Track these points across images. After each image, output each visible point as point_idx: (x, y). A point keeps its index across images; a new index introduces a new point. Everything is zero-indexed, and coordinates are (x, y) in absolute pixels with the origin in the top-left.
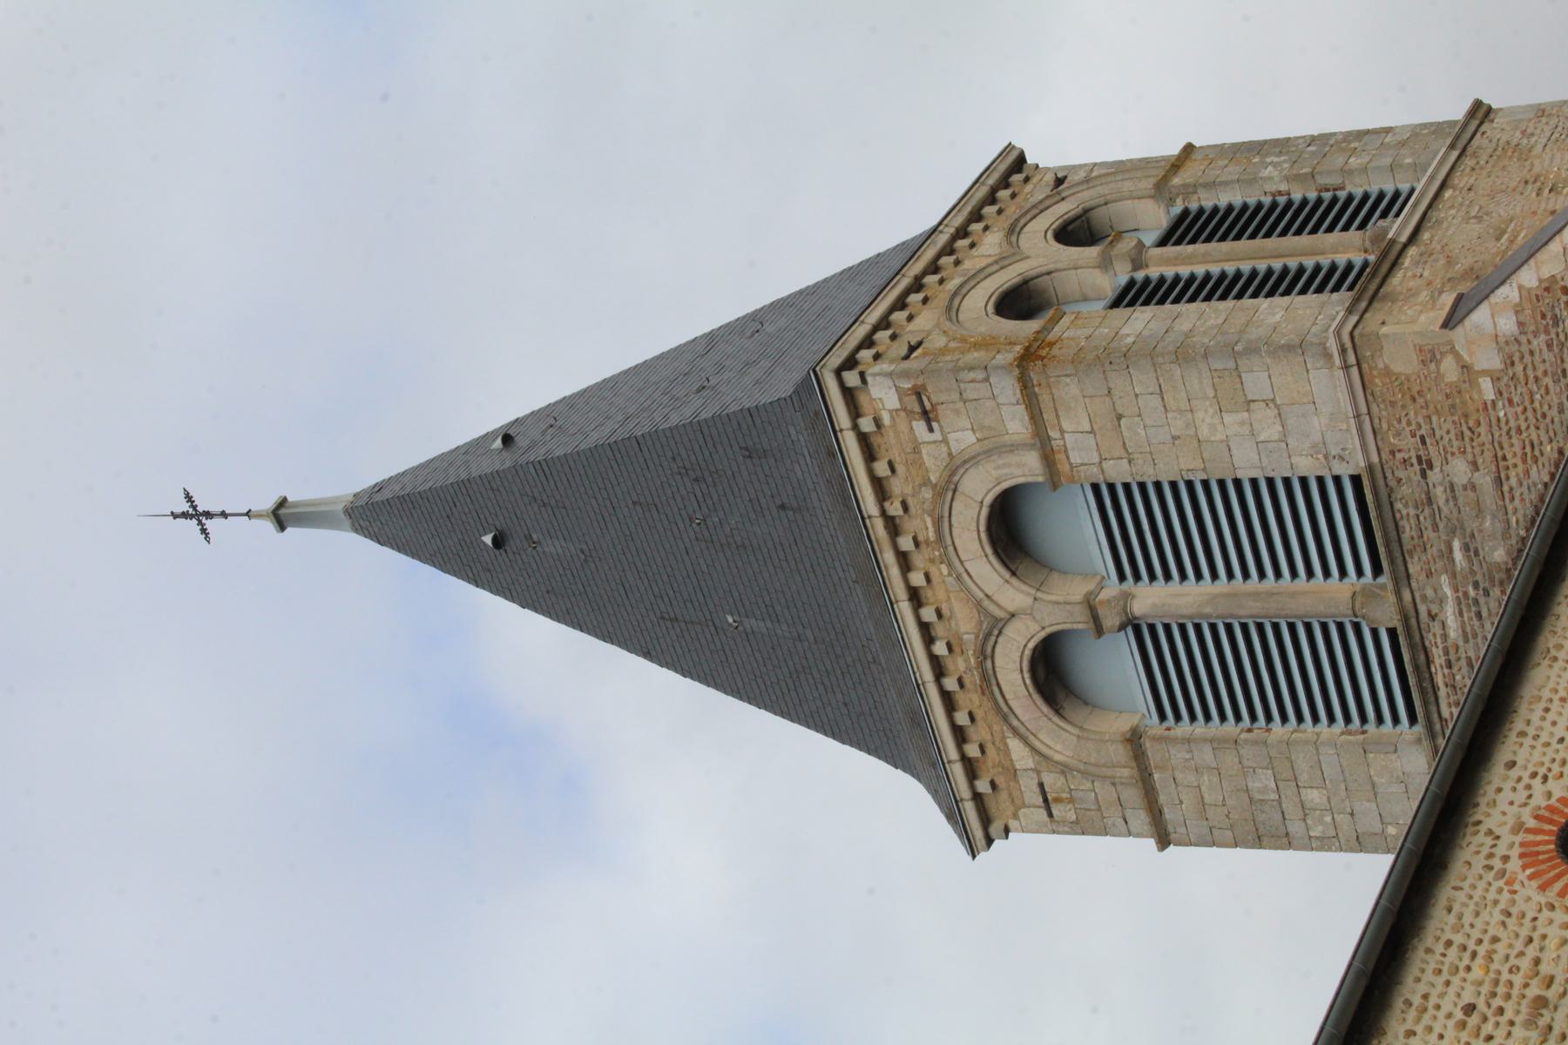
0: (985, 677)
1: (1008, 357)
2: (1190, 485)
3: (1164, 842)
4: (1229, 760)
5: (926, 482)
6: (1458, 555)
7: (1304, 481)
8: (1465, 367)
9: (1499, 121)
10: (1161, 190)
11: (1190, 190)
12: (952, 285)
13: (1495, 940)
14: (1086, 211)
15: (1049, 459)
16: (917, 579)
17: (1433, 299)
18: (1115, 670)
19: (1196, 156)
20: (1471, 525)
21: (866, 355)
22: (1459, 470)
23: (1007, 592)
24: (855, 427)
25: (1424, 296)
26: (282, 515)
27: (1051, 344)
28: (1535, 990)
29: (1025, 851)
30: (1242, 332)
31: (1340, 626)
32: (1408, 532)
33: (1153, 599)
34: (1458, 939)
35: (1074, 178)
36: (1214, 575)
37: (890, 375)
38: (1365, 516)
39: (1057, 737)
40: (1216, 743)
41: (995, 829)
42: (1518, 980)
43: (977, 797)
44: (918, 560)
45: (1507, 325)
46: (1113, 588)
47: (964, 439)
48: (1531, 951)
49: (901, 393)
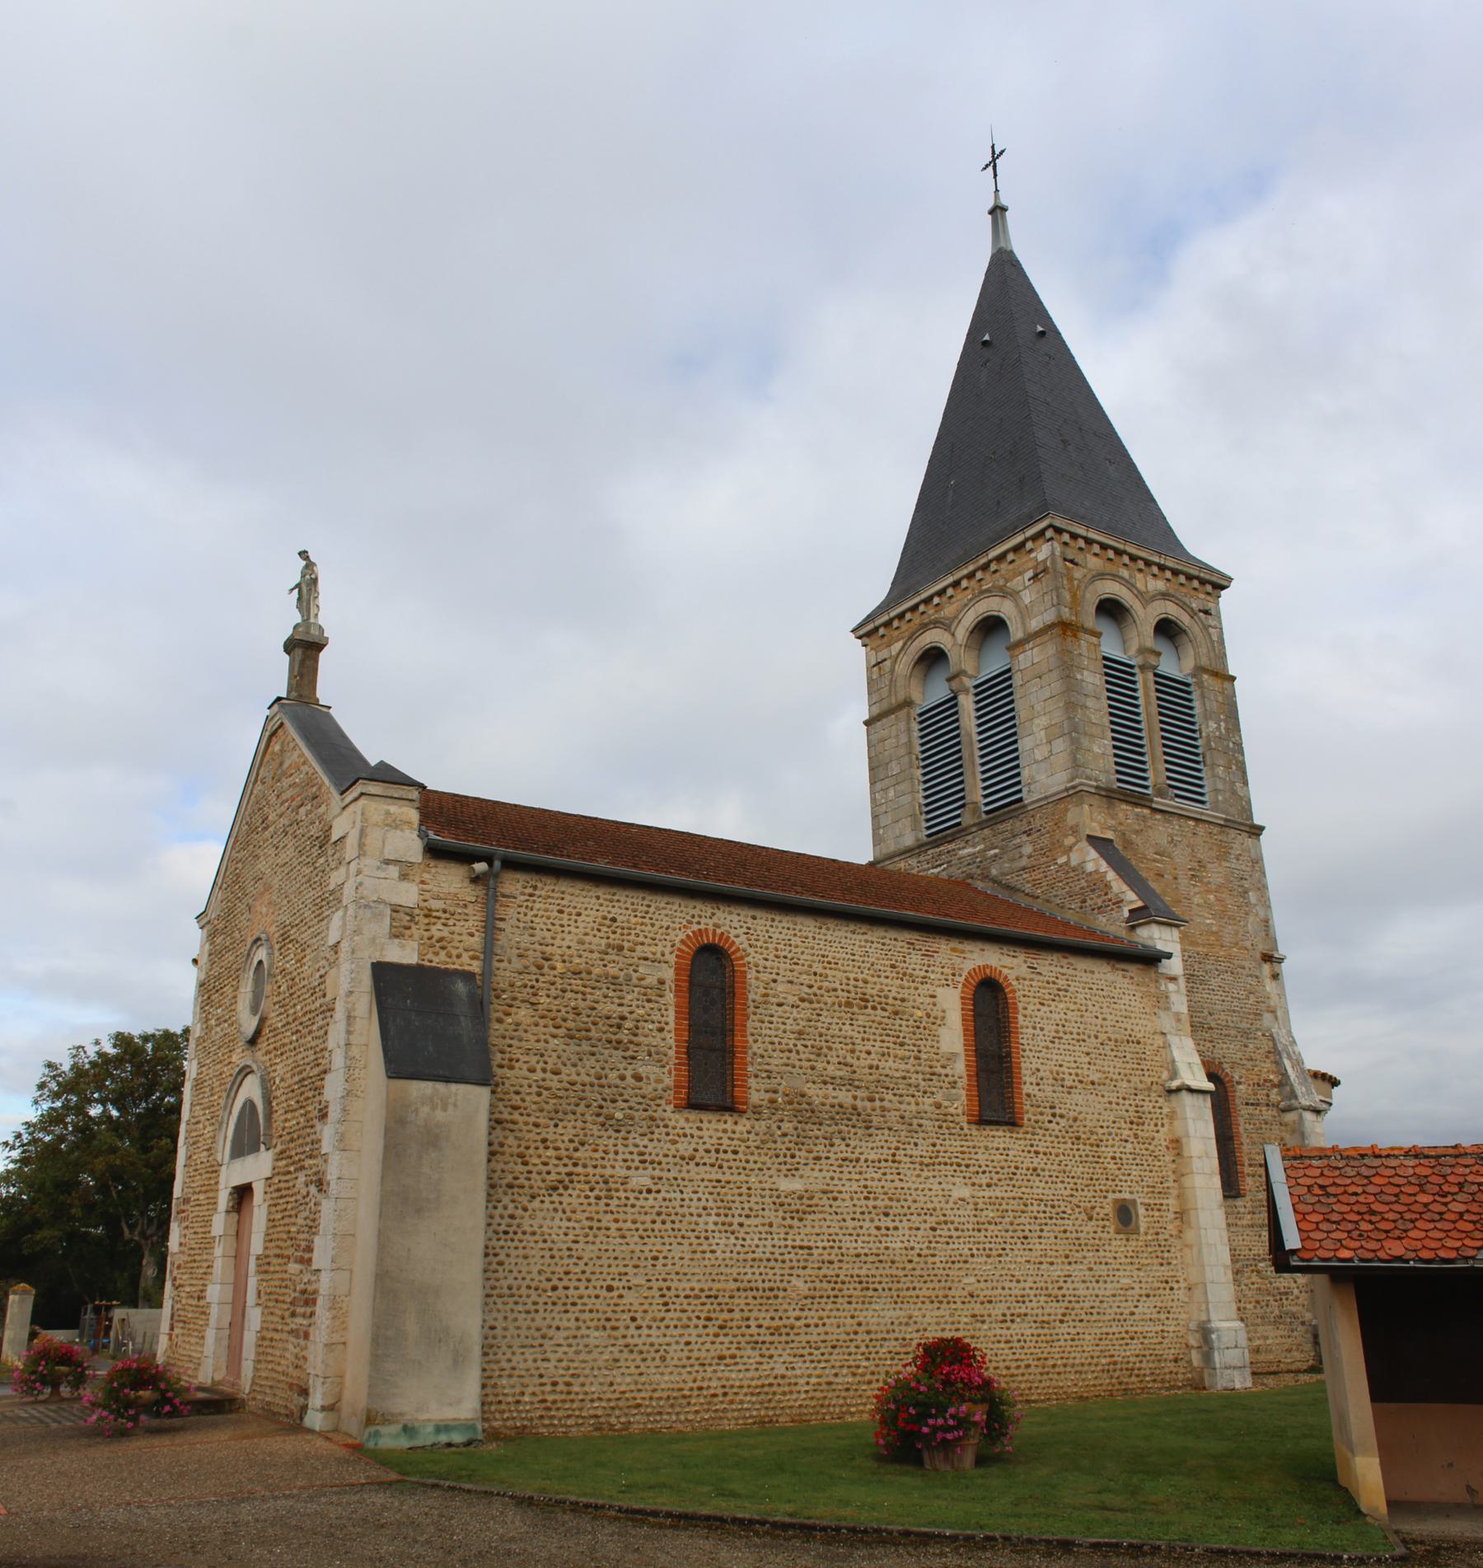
0: (926, 625)
1: (1066, 614)
2: (1013, 718)
3: (867, 723)
4: (902, 751)
5: (1007, 581)
6: (992, 852)
7: (1018, 774)
8: (1071, 848)
9: (1250, 841)
10: (1200, 670)
11: (1200, 685)
12: (1125, 573)
13: (653, 925)
14: (1185, 631)
15: (1020, 643)
16: (964, 583)
17: (1109, 828)
18: (938, 691)
19: (1226, 684)
20: (1005, 858)
21: (1066, 537)
22: (1028, 849)
23: (962, 633)
24: (1027, 540)
25: (1111, 822)
26: (998, 211)
27: (1075, 636)
28: (626, 944)
29: (857, 655)
30: (1086, 734)
31: (963, 798)
32: (1001, 827)
33: (967, 703)
34: (652, 910)
35: (1211, 621)
36: (980, 733)
37: (1053, 554)
38: (1008, 807)
39: (904, 666)
40: (909, 743)
41: (866, 640)
42: (632, 937)
43: (876, 629)
44: (973, 583)
45: (1090, 867)
46: (969, 683)
47: (1027, 597)
48: (648, 941)
49: (1044, 561)
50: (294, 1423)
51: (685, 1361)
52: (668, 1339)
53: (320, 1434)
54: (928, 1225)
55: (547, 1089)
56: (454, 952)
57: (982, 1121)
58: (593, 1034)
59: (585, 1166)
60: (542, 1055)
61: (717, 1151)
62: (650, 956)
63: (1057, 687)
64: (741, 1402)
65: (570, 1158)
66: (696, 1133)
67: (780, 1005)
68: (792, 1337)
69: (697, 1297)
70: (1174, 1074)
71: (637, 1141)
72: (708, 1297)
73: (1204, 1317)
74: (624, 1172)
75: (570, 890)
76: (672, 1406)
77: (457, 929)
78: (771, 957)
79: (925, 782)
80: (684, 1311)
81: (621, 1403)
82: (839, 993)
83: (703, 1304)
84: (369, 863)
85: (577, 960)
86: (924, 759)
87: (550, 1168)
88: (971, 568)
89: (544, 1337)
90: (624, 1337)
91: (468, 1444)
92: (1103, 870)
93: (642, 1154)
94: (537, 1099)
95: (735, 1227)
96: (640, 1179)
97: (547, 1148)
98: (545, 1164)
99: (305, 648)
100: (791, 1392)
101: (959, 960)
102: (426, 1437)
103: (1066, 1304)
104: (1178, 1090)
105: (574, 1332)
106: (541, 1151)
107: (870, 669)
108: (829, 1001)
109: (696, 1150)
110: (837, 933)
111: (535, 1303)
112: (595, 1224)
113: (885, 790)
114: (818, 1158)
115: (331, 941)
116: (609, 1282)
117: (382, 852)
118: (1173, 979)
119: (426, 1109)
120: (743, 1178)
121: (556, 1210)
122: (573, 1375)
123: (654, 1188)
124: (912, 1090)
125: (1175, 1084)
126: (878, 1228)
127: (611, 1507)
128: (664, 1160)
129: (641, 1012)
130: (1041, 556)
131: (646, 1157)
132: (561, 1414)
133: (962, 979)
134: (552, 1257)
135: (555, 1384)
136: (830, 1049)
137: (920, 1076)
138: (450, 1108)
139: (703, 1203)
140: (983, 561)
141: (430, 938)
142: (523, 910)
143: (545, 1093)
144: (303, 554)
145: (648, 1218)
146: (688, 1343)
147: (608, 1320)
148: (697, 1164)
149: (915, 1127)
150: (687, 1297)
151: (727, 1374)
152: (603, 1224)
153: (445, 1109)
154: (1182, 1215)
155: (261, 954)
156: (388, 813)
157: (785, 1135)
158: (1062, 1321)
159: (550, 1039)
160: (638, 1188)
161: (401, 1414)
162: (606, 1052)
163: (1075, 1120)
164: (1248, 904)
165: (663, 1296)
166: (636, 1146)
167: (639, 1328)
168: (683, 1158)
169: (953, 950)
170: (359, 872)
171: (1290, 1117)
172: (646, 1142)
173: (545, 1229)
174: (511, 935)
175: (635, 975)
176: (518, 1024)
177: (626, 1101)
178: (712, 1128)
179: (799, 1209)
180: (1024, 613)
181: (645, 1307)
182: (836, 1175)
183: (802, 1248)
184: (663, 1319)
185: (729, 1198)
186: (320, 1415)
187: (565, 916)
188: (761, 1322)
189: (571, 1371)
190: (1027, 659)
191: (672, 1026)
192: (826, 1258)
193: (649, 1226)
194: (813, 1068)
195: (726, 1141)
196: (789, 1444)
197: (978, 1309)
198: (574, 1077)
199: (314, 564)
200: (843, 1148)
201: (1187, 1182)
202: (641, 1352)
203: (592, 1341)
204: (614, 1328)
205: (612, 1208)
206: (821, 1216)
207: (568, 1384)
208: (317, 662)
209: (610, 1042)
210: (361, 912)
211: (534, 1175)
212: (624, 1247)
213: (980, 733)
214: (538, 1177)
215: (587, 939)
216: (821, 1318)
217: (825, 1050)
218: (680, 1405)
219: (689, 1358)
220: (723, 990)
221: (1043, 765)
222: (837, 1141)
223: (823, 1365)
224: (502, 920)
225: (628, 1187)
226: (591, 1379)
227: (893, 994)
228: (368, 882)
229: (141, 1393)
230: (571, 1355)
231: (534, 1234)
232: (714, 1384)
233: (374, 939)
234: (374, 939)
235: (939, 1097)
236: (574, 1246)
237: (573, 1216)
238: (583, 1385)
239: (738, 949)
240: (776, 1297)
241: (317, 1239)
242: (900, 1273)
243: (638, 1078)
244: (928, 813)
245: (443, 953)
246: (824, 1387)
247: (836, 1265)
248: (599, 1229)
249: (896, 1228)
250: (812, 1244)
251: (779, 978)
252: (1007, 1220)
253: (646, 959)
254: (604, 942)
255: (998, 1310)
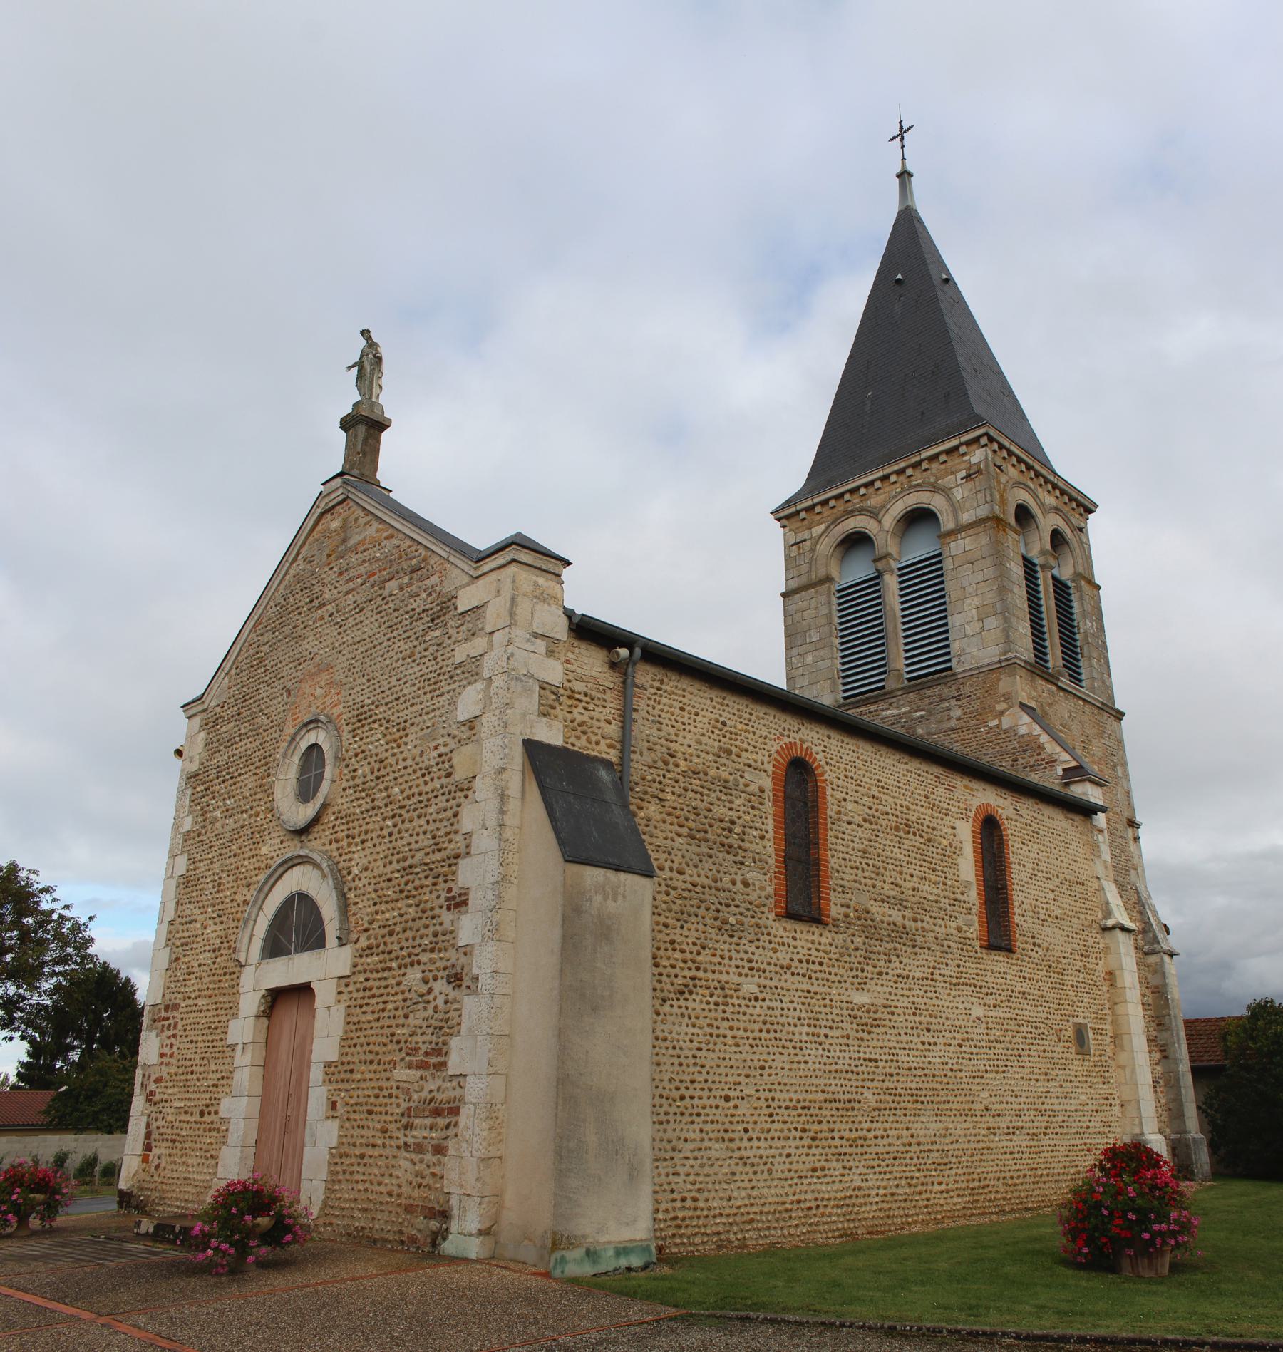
0: (852, 511)
3: (783, 595)
4: (822, 621)
5: (938, 479)
6: (918, 714)
7: (948, 646)
8: (1002, 713)
11: (1079, 589)
12: (1030, 484)
15: (952, 533)
16: (893, 478)
18: (858, 570)
21: (996, 446)
22: (957, 713)
23: (889, 520)
24: (961, 444)
25: (1034, 694)
26: (904, 176)
28: (734, 750)
29: (776, 535)
31: (884, 665)
34: (753, 718)
37: (987, 458)
38: (935, 674)
39: (826, 546)
41: (785, 522)
42: (738, 743)
43: (798, 513)
44: (902, 478)
45: (1023, 730)
46: (895, 565)
47: (958, 494)
48: (751, 748)
50: (429, 1248)
51: (787, 1174)
52: (773, 1151)
53: (478, 1261)
54: (956, 1042)
55: (675, 889)
56: (594, 739)
57: (990, 947)
58: (709, 836)
59: (705, 971)
60: (670, 854)
61: (808, 962)
62: (753, 763)
63: (990, 572)
64: (830, 1215)
65: (693, 961)
66: (792, 942)
67: (850, 823)
68: (865, 1149)
69: (795, 1108)
70: (1108, 914)
71: (746, 947)
72: (803, 1108)
73: (1137, 1131)
74: (736, 979)
75: (690, 689)
76: (777, 1220)
77: (595, 714)
78: (842, 777)
79: (842, 650)
80: (785, 1122)
81: (738, 1219)
82: (890, 817)
83: (800, 1115)
84: (520, 633)
85: (696, 760)
86: (842, 630)
87: (677, 970)
88: (903, 465)
89: (674, 1150)
90: (739, 1149)
91: (645, 1267)
92: (1035, 733)
93: (750, 961)
94: (666, 898)
95: (822, 1038)
96: (749, 987)
97: (674, 950)
98: (673, 967)
99: (365, 427)
100: (866, 1204)
101: (969, 797)
102: (609, 1262)
103: (1046, 1118)
104: (1113, 928)
105: (698, 1144)
106: (670, 953)
107: (788, 547)
108: (884, 823)
109: (792, 960)
110: (887, 761)
111: (667, 1114)
112: (715, 1032)
113: (803, 655)
114: (880, 974)
115: (462, 715)
116: (726, 1092)
117: (531, 625)
118: (1101, 831)
119: (598, 898)
120: (826, 989)
121: (682, 1015)
122: (699, 1190)
123: (761, 996)
124: (942, 914)
125: (1110, 923)
126: (923, 1043)
127: (1004, 1334)
128: (768, 968)
129: (747, 817)
130: (974, 460)
131: (754, 964)
132: (689, 1231)
133: (972, 814)
134: (680, 1065)
135: (684, 1200)
136: (885, 869)
137: (947, 901)
138: (620, 898)
139: (798, 1013)
140: (915, 459)
141: (572, 721)
142: (651, 703)
143: (672, 892)
144: (365, 333)
145: (756, 1027)
146: (789, 1155)
147: (726, 1131)
148: (793, 974)
149: (946, 948)
150: (787, 1108)
151: (818, 1187)
152: (721, 1032)
153: (615, 900)
154: (1115, 1039)
155: (318, 737)
156: (536, 584)
157: (857, 949)
158: (1045, 1134)
159: (676, 838)
160: (747, 995)
161: (583, 1236)
162: (721, 855)
163: (1047, 950)
164: (1117, 776)
165: (768, 1107)
166: (746, 952)
167: (750, 1139)
168: (782, 967)
169: (966, 787)
170: (510, 643)
171: (1152, 959)
172: (753, 949)
173: (674, 1035)
174: (642, 729)
175: (742, 781)
176: (649, 820)
177: (737, 906)
178: (804, 938)
179: (868, 1021)
180: (955, 508)
181: (755, 1118)
182: (893, 991)
183: (870, 1060)
184: (769, 1131)
185: (817, 1009)
186: (477, 1241)
187: (685, 714)
188: (842, 1133)
189: (697, 1186)
190: (956, 547)
191: (771, 834)
192: (888, 1071)
193: (757, 1034)
194: (874, 886)
195: (813, 952)
196: (981, 1252)
197: (992, 1122)
198: (695, 879)
199: (377, 345)
200: (898, 964)
201: (1120, 1009)
202: (753, 1165)
203: (713, 1154)
204: (731, 1140)
205: (728, 1015)
206: (883, 1030)
207: (695, 1200)
208: (379, 442)
209: (723, 845)
210: (513, 684)
211: (664, 978)
212: (738, 1056)
213: (903, 610)
214: (668, 980)
215: (704, 739)
216: (885, 1130)
217: (882, 870)
218: (784, 1220)
219: (790, 1171)
220: (806, 804)
221: (974, 639)
222: (894, 958)
223: (888, 1176)
224: (636, 710)
225: (740, 993)
226: (713, 1193)
227: (927, 823)
228: (518, 653)
229: (259, 1220)
230: (697, 1169)
231: (665, 1039)
232: (810, 1196)
233: (524, 715)
234: (524, 715)
235: (960, 922)
236: (698, 1054)
237: (697, 1022)
238: (707, 1200)
239: (819, 766)
240: (853, 1109)
241: (454, 1042)
242: (939, 1087)
243: (746, 884)
244: (844, 677)
245: (584, 738)
246: (889, 1198)
247: (895, 1078)
248: (718, 1036)
249: (935, 1044)
250: (877, 1057)
251: (848, 797)
252: (1008, 1039)
253: (750, 766)
254: (716, 744)
255: (1003, 1123)
